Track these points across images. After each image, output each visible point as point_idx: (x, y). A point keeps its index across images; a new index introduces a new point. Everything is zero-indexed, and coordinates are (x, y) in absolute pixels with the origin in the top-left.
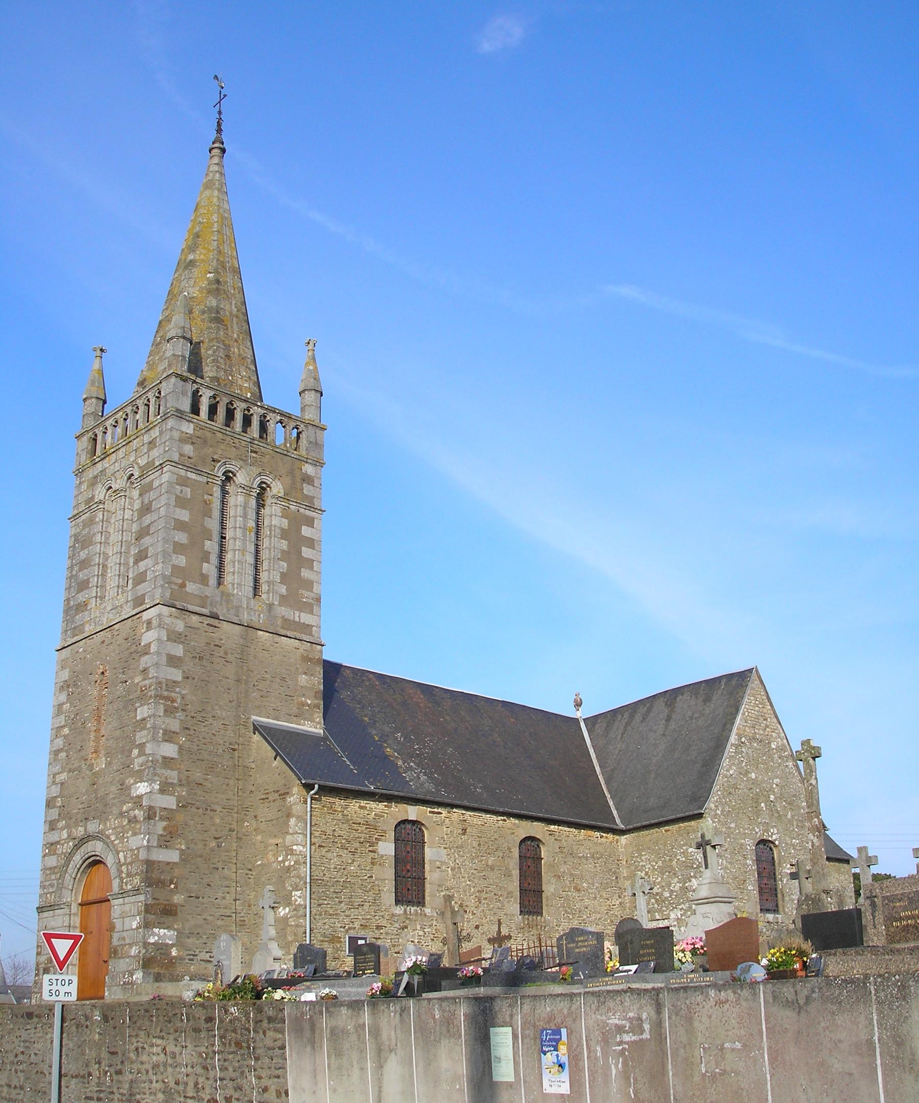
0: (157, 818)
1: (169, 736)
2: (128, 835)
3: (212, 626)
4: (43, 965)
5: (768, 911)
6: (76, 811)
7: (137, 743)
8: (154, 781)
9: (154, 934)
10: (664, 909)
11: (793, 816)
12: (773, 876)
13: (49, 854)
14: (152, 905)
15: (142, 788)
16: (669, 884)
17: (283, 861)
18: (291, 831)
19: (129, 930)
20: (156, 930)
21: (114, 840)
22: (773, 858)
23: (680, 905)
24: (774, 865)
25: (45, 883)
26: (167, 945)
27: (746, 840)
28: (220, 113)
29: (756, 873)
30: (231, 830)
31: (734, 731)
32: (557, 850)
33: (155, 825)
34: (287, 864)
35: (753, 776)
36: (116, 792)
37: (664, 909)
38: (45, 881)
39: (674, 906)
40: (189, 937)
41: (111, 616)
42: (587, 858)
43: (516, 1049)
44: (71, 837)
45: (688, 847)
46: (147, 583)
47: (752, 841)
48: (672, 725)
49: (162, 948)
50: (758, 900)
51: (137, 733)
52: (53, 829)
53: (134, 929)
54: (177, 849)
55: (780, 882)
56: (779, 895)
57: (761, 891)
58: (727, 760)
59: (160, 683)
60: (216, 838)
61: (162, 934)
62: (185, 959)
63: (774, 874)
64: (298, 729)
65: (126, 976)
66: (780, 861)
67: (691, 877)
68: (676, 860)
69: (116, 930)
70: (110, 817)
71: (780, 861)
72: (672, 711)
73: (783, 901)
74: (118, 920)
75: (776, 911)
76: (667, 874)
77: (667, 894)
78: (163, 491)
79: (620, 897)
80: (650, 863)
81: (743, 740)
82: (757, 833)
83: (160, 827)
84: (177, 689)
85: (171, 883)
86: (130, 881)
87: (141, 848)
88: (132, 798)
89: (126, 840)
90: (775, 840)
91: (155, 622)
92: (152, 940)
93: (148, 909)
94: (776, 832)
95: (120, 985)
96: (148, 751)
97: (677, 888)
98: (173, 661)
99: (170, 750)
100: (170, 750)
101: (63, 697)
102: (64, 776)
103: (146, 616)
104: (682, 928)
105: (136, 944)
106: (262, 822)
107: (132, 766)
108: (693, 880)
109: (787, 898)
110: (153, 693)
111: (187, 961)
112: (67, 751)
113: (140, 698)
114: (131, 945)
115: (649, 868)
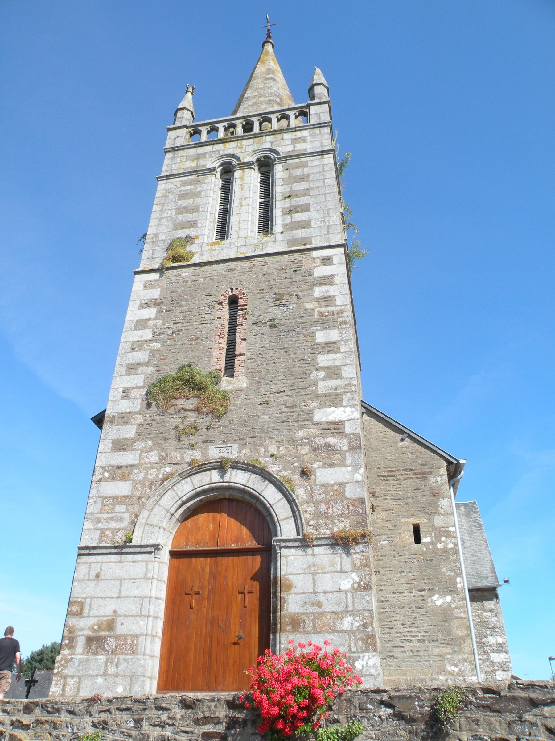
34: (439, 546)
38: (101, 513)
51: (319, 356)
53: (346, 592)
69: (293, 590)
87: (348, 483)
105: (354, 613)
113: (317, 323)
114: (339, 615)
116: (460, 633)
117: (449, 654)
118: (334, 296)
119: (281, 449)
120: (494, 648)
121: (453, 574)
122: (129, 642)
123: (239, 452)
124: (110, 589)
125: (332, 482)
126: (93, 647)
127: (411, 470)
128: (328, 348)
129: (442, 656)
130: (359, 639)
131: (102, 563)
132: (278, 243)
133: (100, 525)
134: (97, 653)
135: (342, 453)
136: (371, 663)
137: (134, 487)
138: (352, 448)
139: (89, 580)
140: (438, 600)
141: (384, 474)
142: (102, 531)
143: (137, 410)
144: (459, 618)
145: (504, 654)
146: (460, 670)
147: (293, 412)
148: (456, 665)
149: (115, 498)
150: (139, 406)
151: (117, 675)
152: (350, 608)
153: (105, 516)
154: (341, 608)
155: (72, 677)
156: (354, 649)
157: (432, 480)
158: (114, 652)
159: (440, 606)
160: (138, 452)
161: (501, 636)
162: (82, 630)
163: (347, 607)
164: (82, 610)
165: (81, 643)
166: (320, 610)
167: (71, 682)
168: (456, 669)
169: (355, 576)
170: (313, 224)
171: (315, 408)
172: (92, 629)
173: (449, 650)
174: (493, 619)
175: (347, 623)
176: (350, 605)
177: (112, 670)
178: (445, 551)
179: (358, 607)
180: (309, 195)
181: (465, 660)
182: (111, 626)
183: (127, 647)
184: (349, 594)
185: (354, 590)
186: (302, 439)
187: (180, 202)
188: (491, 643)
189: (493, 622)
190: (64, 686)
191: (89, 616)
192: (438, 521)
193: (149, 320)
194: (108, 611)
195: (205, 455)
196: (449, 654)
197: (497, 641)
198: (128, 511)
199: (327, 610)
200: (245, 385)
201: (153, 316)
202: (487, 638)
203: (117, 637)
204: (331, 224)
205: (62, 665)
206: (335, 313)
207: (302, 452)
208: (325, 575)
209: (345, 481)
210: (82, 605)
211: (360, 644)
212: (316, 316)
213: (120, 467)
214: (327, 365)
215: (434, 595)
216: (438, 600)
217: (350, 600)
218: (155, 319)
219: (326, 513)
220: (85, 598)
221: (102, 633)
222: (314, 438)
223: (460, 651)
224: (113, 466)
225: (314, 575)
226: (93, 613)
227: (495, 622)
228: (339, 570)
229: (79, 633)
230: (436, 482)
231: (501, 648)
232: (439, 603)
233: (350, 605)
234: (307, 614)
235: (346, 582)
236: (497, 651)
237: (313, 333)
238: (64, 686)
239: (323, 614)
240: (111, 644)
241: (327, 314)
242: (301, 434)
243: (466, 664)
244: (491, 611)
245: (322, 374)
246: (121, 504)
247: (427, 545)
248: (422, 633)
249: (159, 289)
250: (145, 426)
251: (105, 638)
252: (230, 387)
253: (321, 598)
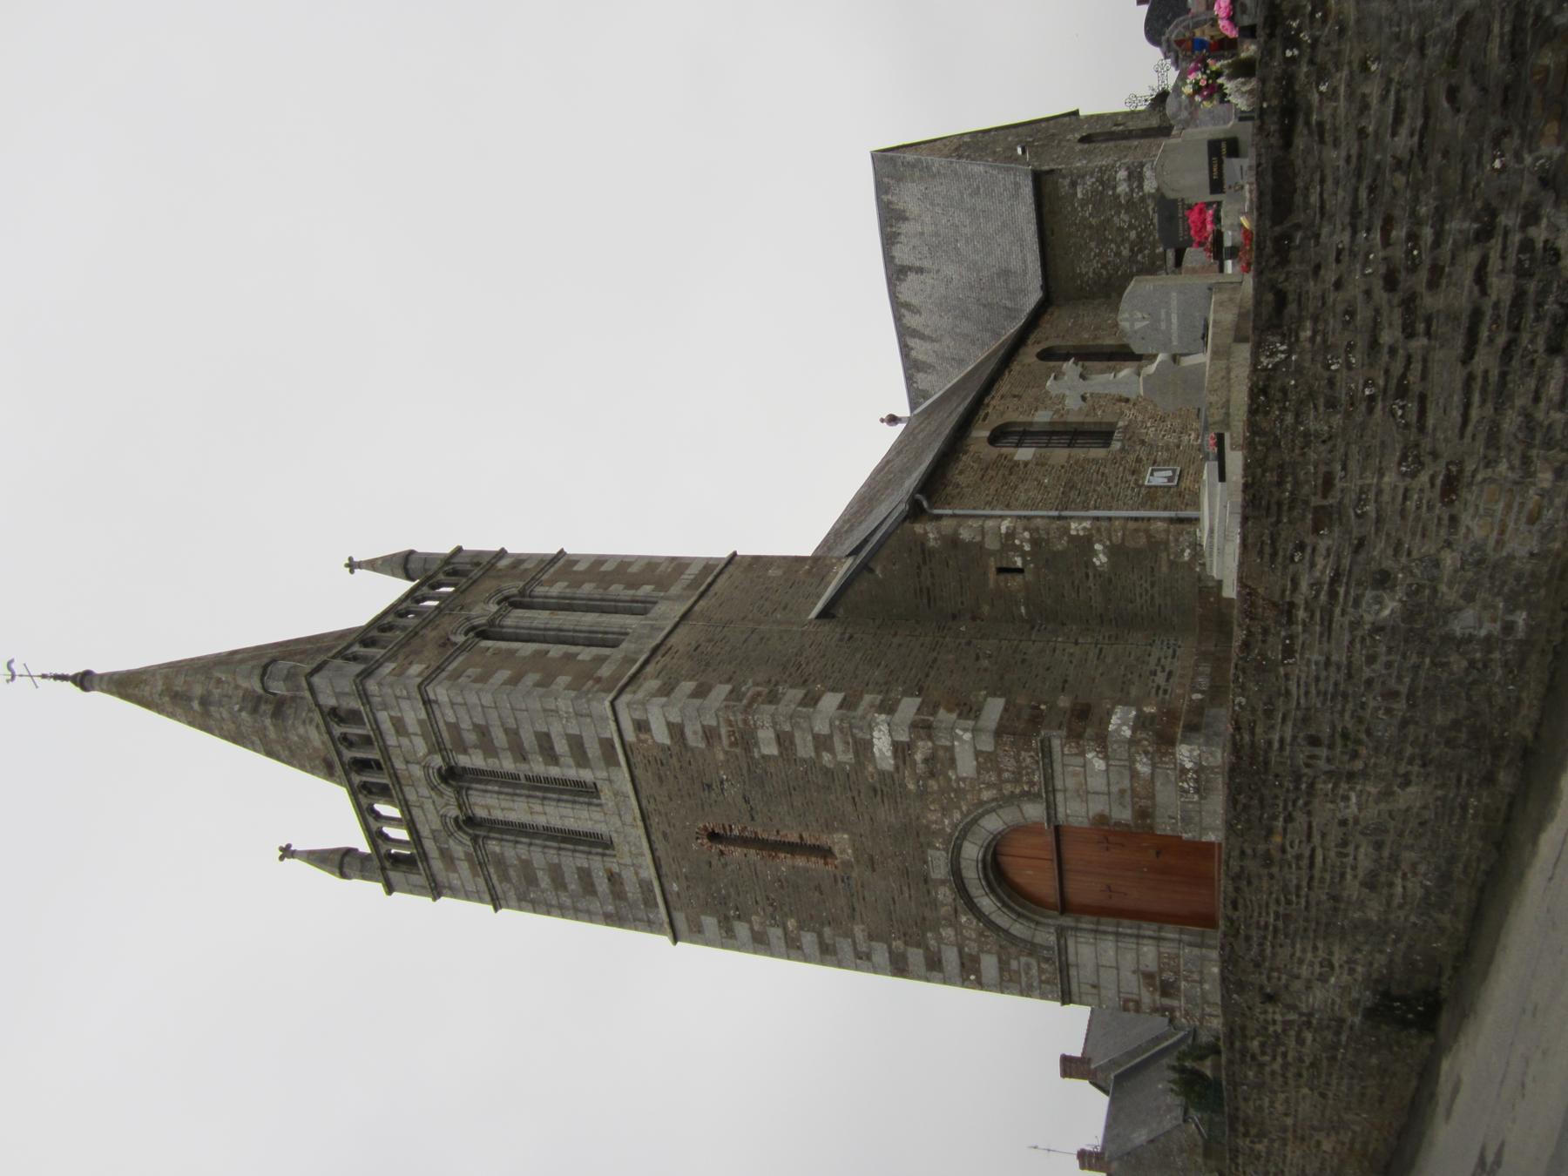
0: (931, 718)
1: (811, 700)
2: (954, 777)
3: (666, 653)
4: (1157, 997)
6: (913, 904)
7: (813, 754)
8: (873, 719)
9: (1118, 730)
10: (1151, 238)
13: (978, 972)
14: (1070, 730)
15: (882, 744)
16: (1120, 229)
17: (1023, 555)
18: (978, 539)
19: (1108, 778)
20: (1111, 728)
21: (962, 812)
23: (1148, 212)
25: (1023, 984)
26: (1137, 717)
28: (44, 676)
30: (969, 643)
33: (941, 722)
34: (1027, 548)
36: (887, 807)
37: (1151, 238)
38: (1020, 983)
40: (1128, 693)
41: (628, 819)
43: (1327, 618)
44: (953, 922)
46: (584, 734)
48: (926, 264)
49: (1141, 723)
51: (799, 755)
52: (940, 961)
53: (1108, 766)
54: (985, 700)
59: (726, 707)
60: (978, 658)
61: (1120, 722)
62: (1163, 699)
65: (1186, 785)
67: (1114, 193)
69: (1107, 812)
70: (924, 821)
72: (910, 269)
74: (1091, 805)
77: (1133, 234)
78: (460, 700)
80: (1091, 260)
83: (945, 716)
84: (743, 689)
85: (1037, 708)
86: (1028, 774)
87: (975, 748)
88: (897, 768)
89: (962, 785)
91: (638, 715)
92: (1127, 732)
93: (1075, 736)
95: (1198, 803)
96: (825, 730)
97: (1126, 218)
98: (701, 692)
99: (831, 701)
100: (831, 701)
101: (742, 929)
102: (859, 931)
103: (630, 736)
105: (1132, 761)
106: (962, 603)
107: (848, 768)
110: (740, 717)
111: (1167, 697)
112: (822, 925)
113: (748, 749)
114: (1134, 774)
115: (1097, 262)
116: (1143, 541)
117: (1168, 555)
118: (703, 726)
119: (932, 808)
120: (1135, 185)
121: (1065, 538)
122: (1166, 960)
123: (938, 849)
124: (1108, 977)
125: (975, 763)
126: (1172, 991)
127: (919, 567)
128: (787, 744)
129: (1172, 564)
130: (1161, 759)
131: (1079, 983)
132: (613, 778)
133: (1035, 984)
134: (1178, 989)
135: (935, 749)
136: (1187, 754)
137: (989, 952)
138: (930, 737)
139: (1099, 995)
140: (1101, 559)
141: (925, 601)
142: (1041, 982)
143: (885, 946)
144: (1123, 539)
145: (1145, 169)
146: (1188, 547)
147: (882, 791)
148: (1183, 551)
149: (1001, 970)
150: (881, 944)
151: (1201, 972)
152: (1127, 763)
153: (1024, 979)
154: (1127, 773)
155: (1203, 1009)
156: (1172, 766)
157: (932, 543)
158: (1177, 973)
159: (1108, 557)
160: (943, 947)
161: (1116, 172)
162: (1154, 1001)
163: (1124, 766)
164: (1132, 1000)
165: (1167, 1002)
166: (1129, 792)
167: (1208, 1010)
168: (1188, 551)
169: (1089, 756)
170: (575, 731)
171: (876, 767)
172: (1153, 993)
173: (1164, 555)
174: (1089, 183)
175: (1143, 768)
176: (1122, 763)
177: (1196, 977)
178: (1035, 542)
179: (1126, 756)
180: (518, 728)
181: (1177, 540)
182: (1149, 977)
183: (1172, 963)
184: (1111, 762)
185: (1106, 758)
186: (919, 786)
187: (543, 885)
188: (1127, 190)
189: (1093, 183)
190: (1212, 1016)
191: (1139, 995)
192: (992, 544)
193: (752, 929)
194: (1133, 978)
195: (943, 882)
196: (1168, 555)
197: (1124, 180)
198: (1017, 958)
199: (1129, 785)
200: (846, 836)
201: (746, 926)
202: (1119, 196)
203: (1161, 970)
204: (571, 710)
205: (1191, 1018)
206: (730, 729)
207: (936, 788)
208: (1089, 783)
209: (972, 750)
210: (1127, 1001)
211: (1166, 759)
212: (738, 750)
213: (963, 965)
214: (812, 748)
215: (1094, 563)
216: (1101, 559)
217: (1117, 763)
218: (750, 922)
219: (1013, 773)
220: (1119, 998)
221: (1158, 983)
222: (916, 773)
223: (1167, 543)
224: (961, 971)
225: (1088, 792)
226: (1136, 990)
227: (1094, 180)
228: (1082, 769)
229: (1158, 1002)
230: (935, 539)
231: (1135, 174)
232: (1104, 559)
233: (1122, 763)
234: (1134, 804)
235: (1097, 765)
236: (1141, 178)
237: (763, 757)
238: (1212, 1016)
239: (1133, 789)
240: (1168, 976)
241: (733, 739)
242: (911, 786)
243: (1181, 539)
244: (1074, 184)
245: (826, 757)
246: (1008, 963)
247: (1025, 562)
248: (1143, 581)
249: (703, 917)
250: (908, 938)
251: (1162, 981)
252: (850, 851)
253: (1114, 789)
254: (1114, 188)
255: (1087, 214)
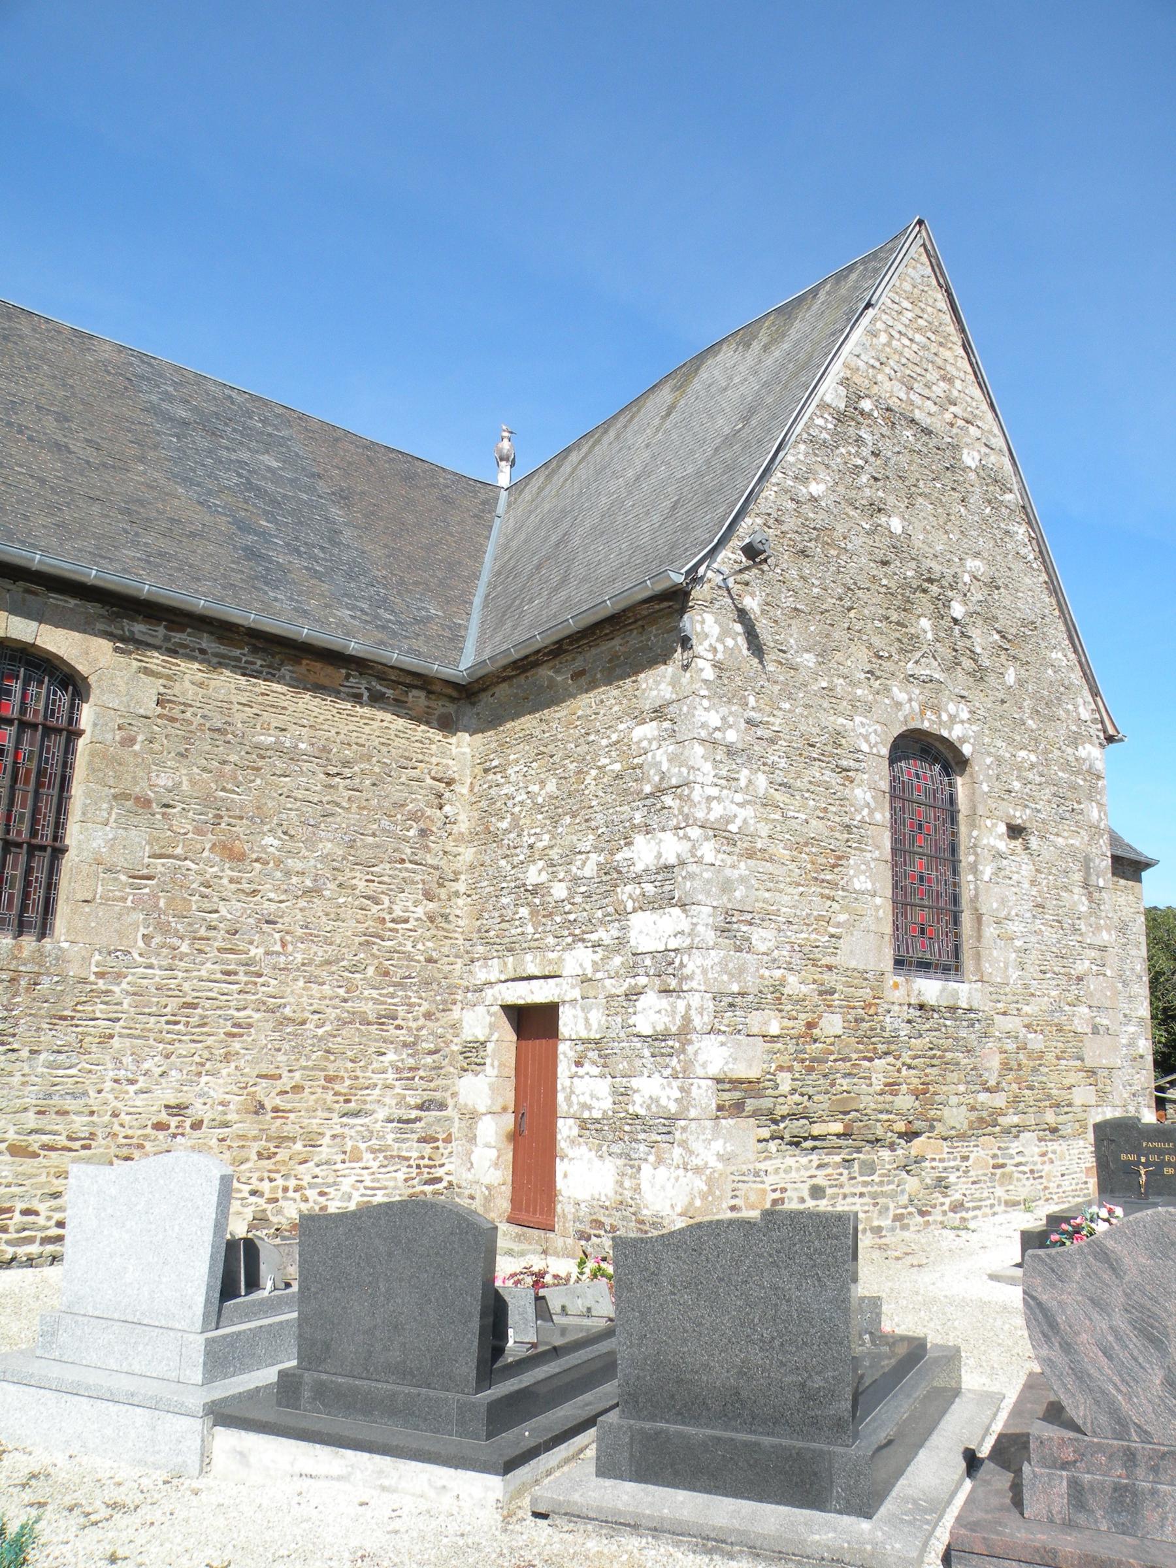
5: (924, 966)
11: (1021, 683)
12: (948, 855)
22: (952, 800)
24: (953, 820)
27: (858, 719)
29: (887, 834)
31: (837, 369)
32: (149, 706)
35: (896, 525)
37: (551, 940)
39: (577, 932)
42: (293, 756)
45: (631, 723)
47: (878, 727)
50: (888, 929)
55: (971, 877)
56: (966, 918)
57: (901, 904)
58: (802, 447)
63: (954, 849)
64: (62, 569)
66: (974, 808)
67: (634, 827)
68: (594, 772)
71: (974, 808)
73: (979, 938)
75: (951, 967)
76: (567, 820)
79: (429, 896)
81: (866, 405)
82: (898, 705)
90: (963, 740)
94: (965, 715)
104: (594, 1011)
108: (639, 840)
109: (990, 931)
120: (649, 888)
145: (676, 911)
244: (659, 713)
254: (647, 830)
255: (604, 761)
